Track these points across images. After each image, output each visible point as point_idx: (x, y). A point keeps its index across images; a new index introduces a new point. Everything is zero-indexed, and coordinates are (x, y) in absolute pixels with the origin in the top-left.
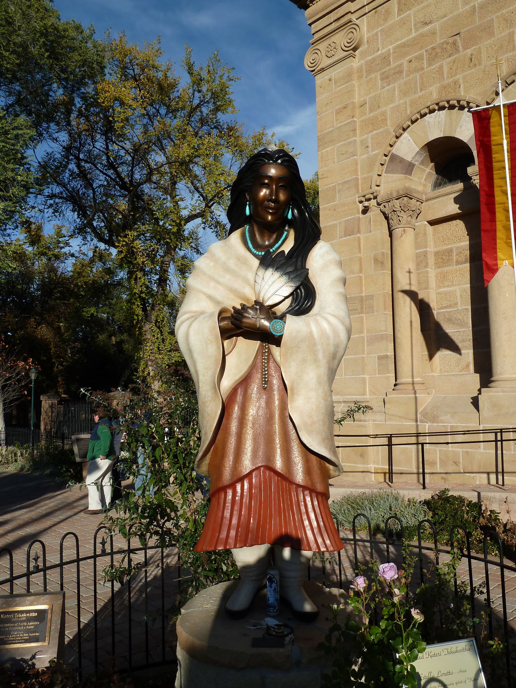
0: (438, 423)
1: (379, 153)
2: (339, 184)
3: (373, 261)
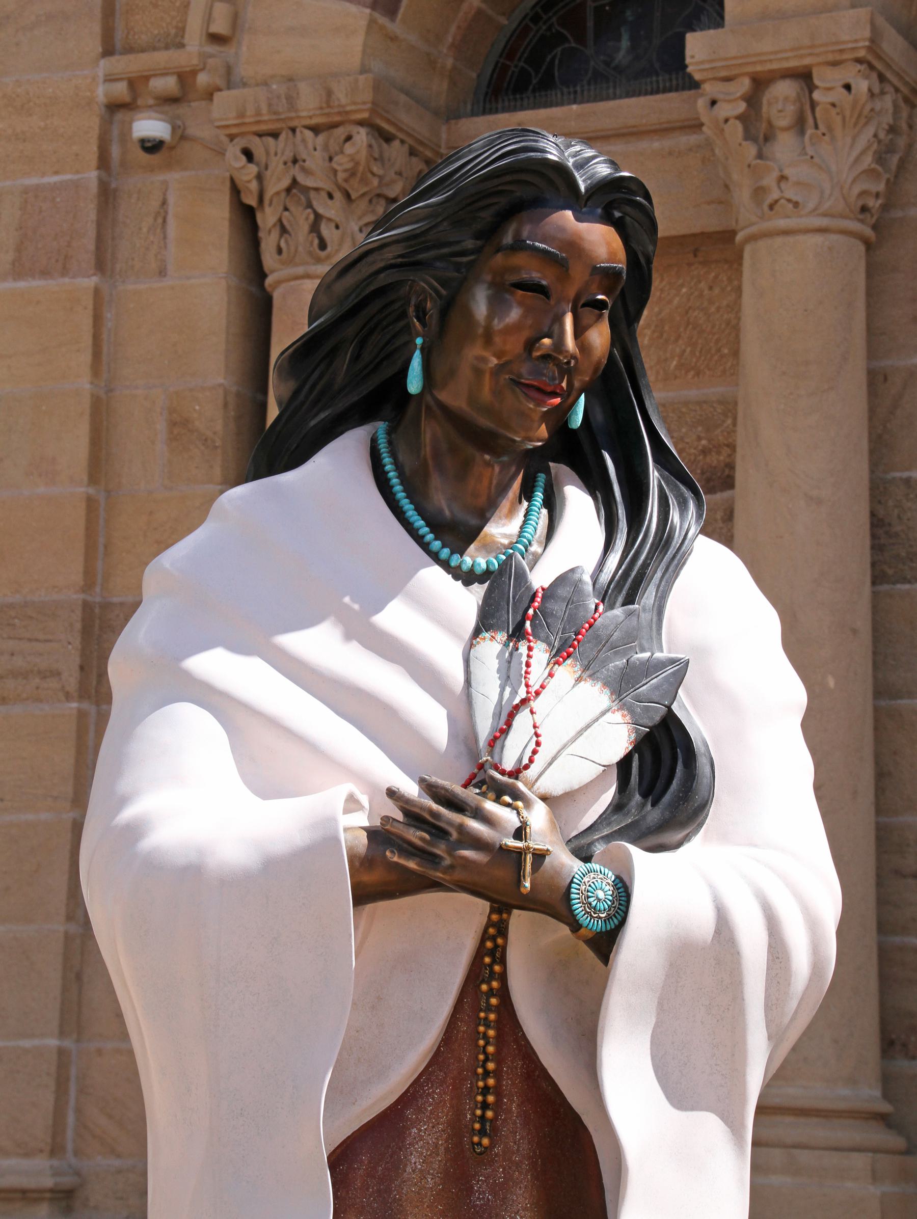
3: (161, 426)
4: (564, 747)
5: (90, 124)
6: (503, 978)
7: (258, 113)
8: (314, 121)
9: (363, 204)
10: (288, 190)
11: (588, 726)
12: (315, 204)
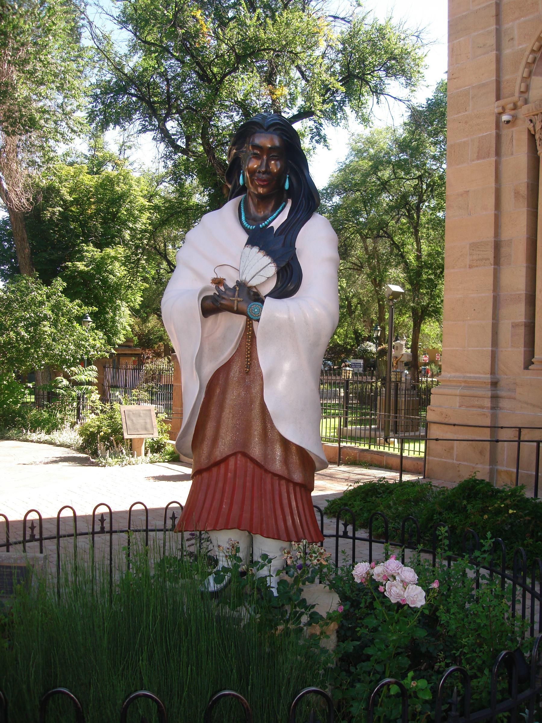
3: (513, 194)
5: (493, 119)
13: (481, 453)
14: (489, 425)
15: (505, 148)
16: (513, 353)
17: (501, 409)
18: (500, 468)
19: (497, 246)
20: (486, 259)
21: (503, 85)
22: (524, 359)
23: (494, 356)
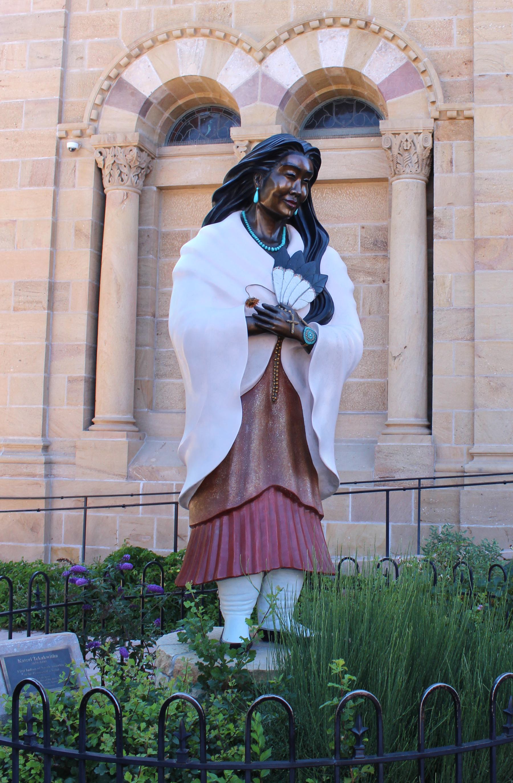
0: (158, 480)
1: (101, 73)
2: (28, 102)
4: (299, 297)
6: (280, 357)
7: (105, 141)
8: (121, 145)
9: (135, 169)
10: (113, 164)
11: (305, 292)
12: (120, 168)
13: (33, 529)
14: (44, 495)
15: (64, 178)
16: (70, 411)
17: (55, 476)
18: (55, 545)
19: (52, 288)
20: (37, 302)
21: (65, 107)
22: (84, 418)
23: (45, 415)
